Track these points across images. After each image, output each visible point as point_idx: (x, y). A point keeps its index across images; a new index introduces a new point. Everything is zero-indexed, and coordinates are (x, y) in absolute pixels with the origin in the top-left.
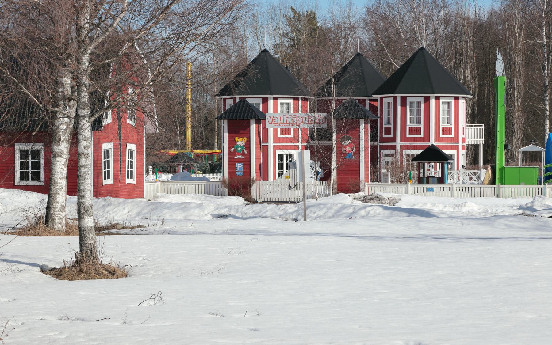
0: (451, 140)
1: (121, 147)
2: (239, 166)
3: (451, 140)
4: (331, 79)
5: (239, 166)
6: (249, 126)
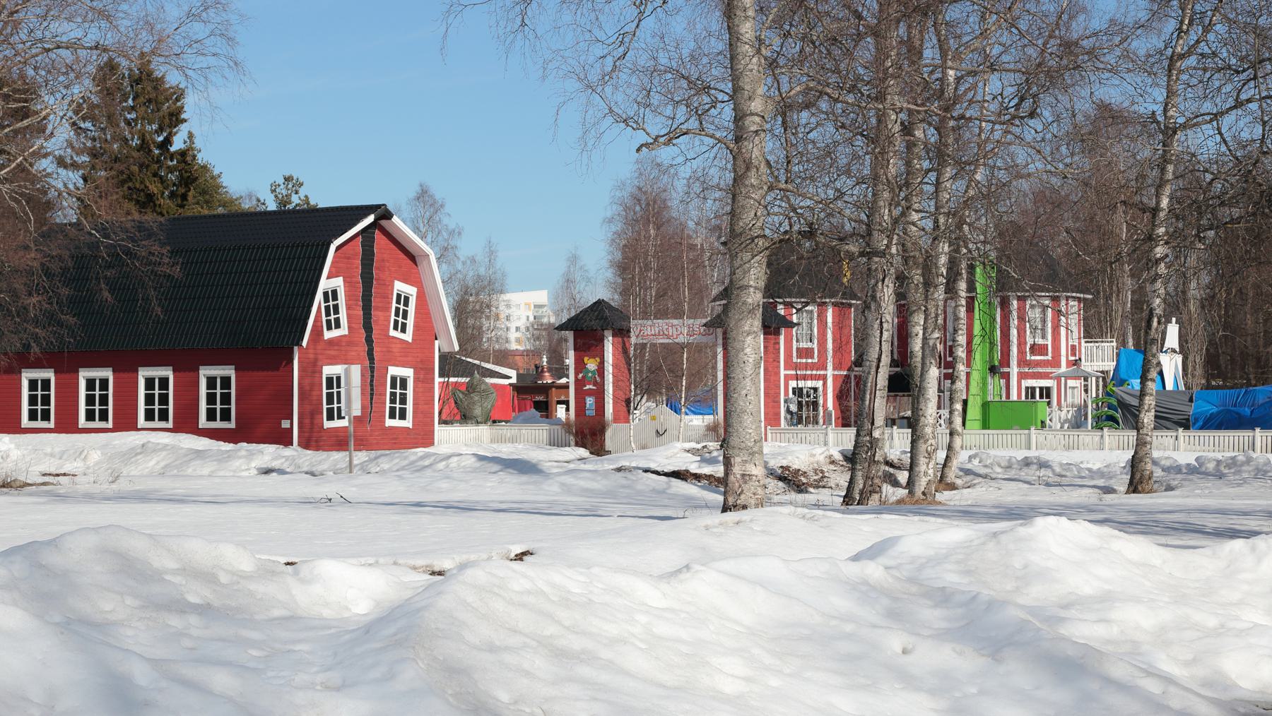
0: (812, 367)
1: (372, 372)
2: (590, 401)
3: (812, 367)
4: (328, 278)
5: (590, 401)
6: (601, 341)
